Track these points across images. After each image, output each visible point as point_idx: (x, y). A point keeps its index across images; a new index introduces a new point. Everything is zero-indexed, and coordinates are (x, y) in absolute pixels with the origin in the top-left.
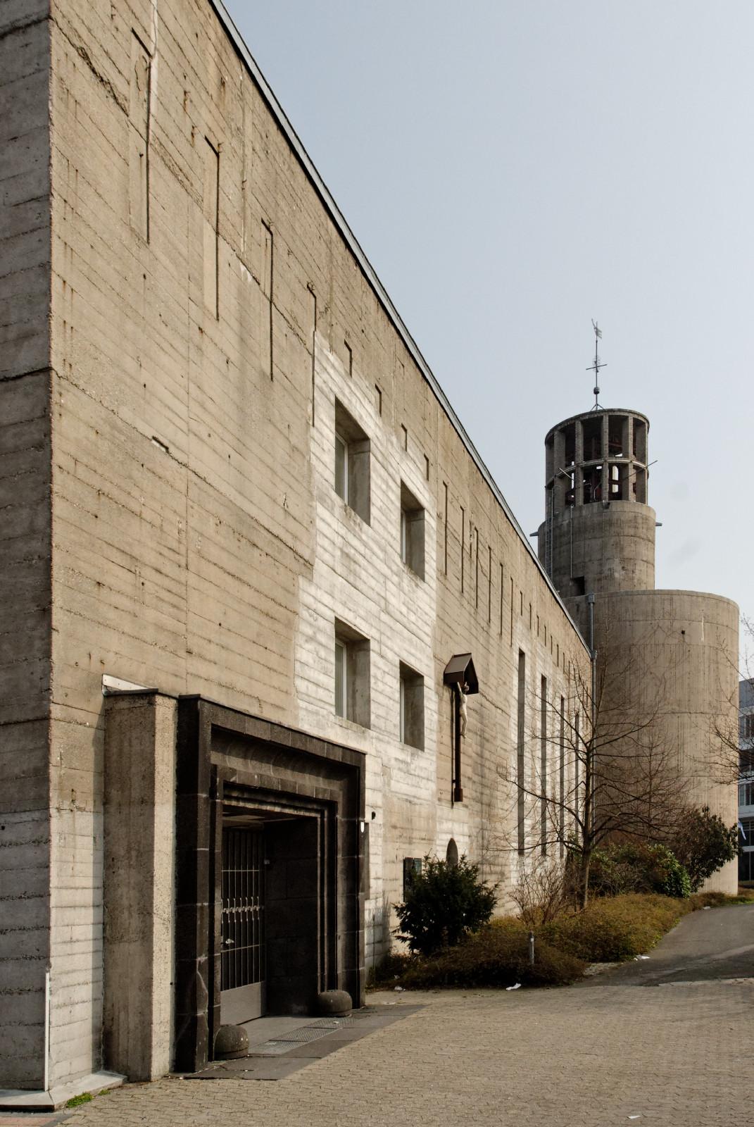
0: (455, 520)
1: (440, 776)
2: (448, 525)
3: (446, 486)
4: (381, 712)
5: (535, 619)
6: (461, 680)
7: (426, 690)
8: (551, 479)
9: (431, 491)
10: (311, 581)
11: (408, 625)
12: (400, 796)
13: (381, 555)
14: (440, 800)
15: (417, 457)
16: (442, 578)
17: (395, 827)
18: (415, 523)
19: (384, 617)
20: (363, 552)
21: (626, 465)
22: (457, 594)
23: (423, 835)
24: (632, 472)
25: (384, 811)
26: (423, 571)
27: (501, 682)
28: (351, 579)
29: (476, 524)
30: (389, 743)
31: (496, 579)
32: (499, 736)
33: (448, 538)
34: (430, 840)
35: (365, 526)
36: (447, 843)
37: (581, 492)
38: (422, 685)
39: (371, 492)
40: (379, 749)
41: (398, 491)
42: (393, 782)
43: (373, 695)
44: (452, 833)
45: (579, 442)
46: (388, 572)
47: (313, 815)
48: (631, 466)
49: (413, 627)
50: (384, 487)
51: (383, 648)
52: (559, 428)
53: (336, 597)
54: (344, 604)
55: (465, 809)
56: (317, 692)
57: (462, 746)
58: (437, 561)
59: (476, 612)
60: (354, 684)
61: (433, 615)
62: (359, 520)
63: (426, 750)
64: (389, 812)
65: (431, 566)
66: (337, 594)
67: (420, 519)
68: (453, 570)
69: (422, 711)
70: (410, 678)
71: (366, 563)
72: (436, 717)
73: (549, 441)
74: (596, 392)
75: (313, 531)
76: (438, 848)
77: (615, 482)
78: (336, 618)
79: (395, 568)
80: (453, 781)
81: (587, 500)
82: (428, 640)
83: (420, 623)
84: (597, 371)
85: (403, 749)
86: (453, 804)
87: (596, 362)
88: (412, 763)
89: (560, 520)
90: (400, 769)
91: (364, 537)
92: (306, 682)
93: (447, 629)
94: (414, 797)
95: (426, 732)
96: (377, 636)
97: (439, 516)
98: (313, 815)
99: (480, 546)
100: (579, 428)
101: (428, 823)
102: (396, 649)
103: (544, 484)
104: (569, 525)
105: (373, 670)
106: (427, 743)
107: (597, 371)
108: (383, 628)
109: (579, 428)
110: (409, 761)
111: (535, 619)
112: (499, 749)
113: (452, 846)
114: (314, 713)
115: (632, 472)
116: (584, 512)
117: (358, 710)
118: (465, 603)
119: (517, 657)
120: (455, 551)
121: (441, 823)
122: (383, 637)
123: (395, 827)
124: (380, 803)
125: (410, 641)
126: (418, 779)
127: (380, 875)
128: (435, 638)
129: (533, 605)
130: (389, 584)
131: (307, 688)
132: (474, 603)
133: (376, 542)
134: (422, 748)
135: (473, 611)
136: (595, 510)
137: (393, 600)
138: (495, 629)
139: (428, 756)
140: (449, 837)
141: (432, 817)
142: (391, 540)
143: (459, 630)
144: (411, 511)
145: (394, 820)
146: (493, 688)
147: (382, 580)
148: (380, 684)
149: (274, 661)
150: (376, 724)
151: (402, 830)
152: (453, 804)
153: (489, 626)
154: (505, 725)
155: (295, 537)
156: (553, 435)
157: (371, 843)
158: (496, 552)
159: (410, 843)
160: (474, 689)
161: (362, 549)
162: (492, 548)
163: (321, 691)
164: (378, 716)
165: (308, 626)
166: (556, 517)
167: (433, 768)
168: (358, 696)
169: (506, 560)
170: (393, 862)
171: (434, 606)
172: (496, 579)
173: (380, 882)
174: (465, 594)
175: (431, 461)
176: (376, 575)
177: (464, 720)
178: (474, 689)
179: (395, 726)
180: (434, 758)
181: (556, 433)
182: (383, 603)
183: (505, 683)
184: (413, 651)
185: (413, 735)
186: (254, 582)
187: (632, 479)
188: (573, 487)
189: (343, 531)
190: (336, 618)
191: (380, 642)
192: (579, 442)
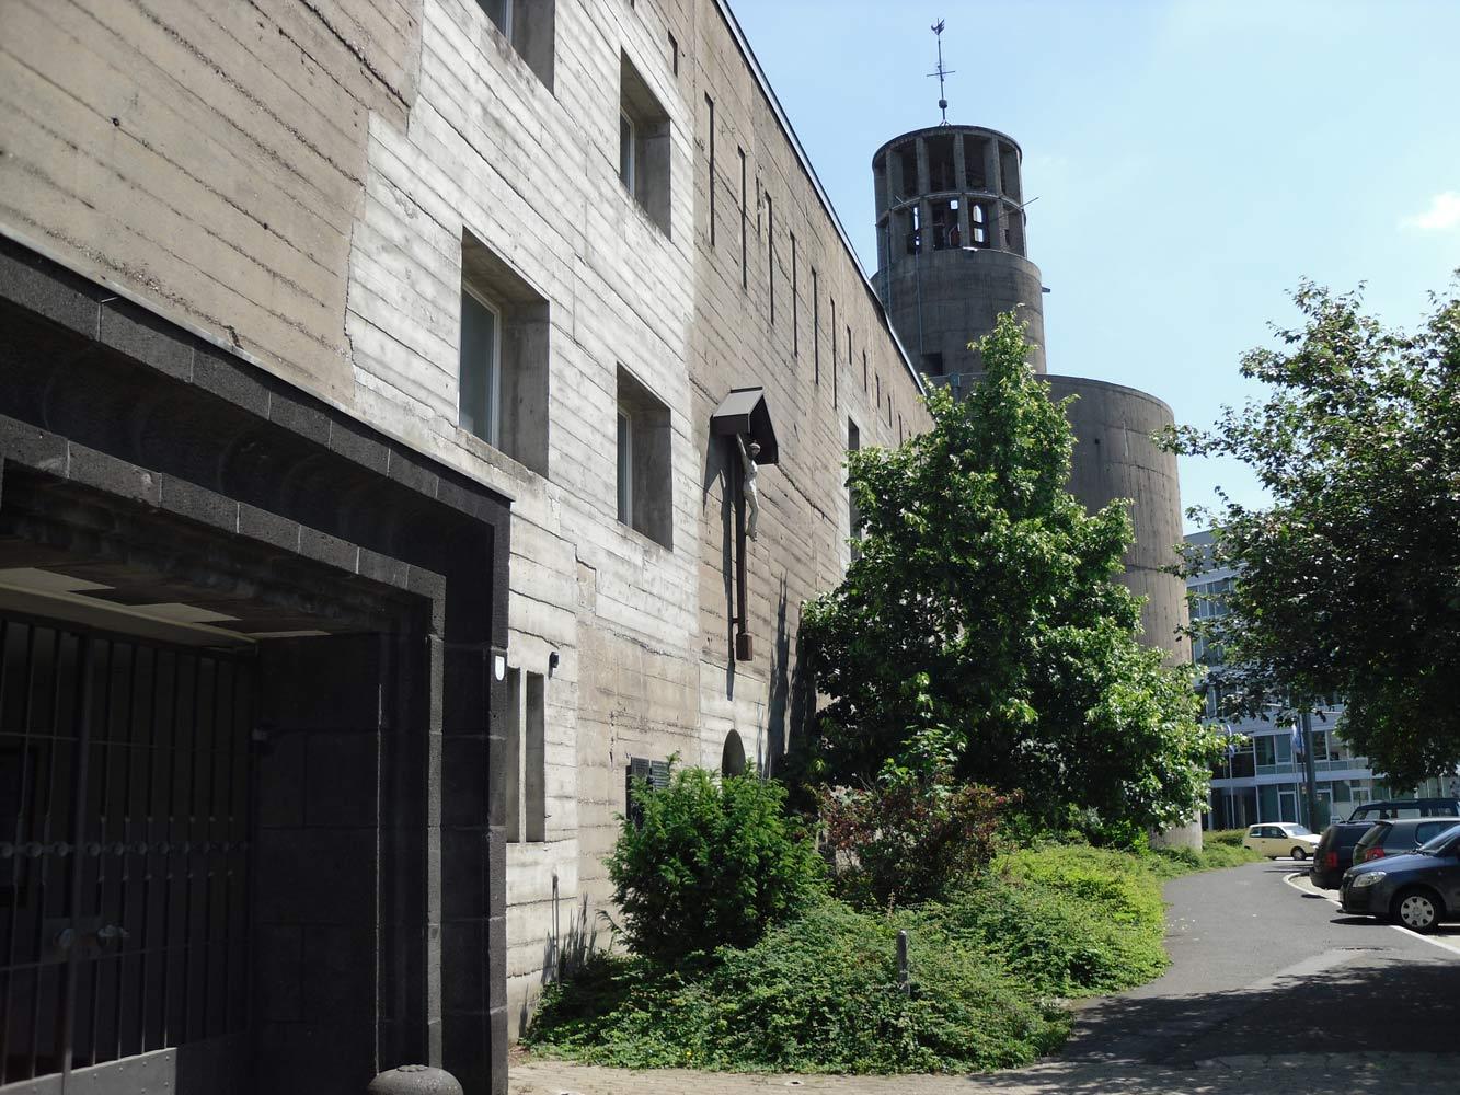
0: (729, 165)
1: (707, 606)
2: (715, 166)
3: (711, 104)
4: (576, 451)
5: (872, 380)
6: (741, 442)
7: (674, 436)
8: (884, 215)
9: (681, 94)
10: (403, 132)
11: (635, 304)
12: (618, 630)
13: (579, 157)
14: (706, 652)
15: (655, 28)
16: (705, 248)
17: (607, 692)
18: (651, 141)
19: (579, 267)
20: (538, 137)
21: (993, 202)
22: (736, 289)
23: (672, 716)
24: (1001, 212)
25: (581, 656)
26: (669, 221)
27: (819, 464)
28: (507, 171)
29: (767, 186)
30: (591, 517)
31: (805, 289)
32: (820, 557)
33: (716, 185)
34: (687, 731)
35: (541, 88)
36: (723, 739)
37: (928, 234)
38: (668, 425)
39: (557, 39)
40: (568, 523)
41: (617, 66)
42: (601, 600)
43: (553, 410)
44: (734, 720)
45: (922, 166)
46: (594, 195)
47: (401, 575)
48: (1000, 206)
49: (644, 311)
50: (586, 42)
51: (579, 306)
52: (892, 146)
53: (466, 188)
54: (488, 212)
55: (756, 677)
56: (408, 364)
57: (749, 559)
58: (697, 214)
59: (772, 330)
60: (515, 385)
61: (690, 307)
62: (527, 71)
63: (675, 549)
64: (592, 659)
65: (682, 218)
66: (469, 184)
67: (663, 136)
68: (729, 240)
69: (668, 475)
70: (641, 413)
71: (542, 156)
72: (694, 529)
73: (879, 163)
74: (943, 105)
75: (415, 42)
76: (704, 746)
77: (978, 225)
78: (466, 231)
79: (606, 189)
80: (732, 621)
81: (939, 244)
82: (679, 347)
83: (661, 310)
84: (942, 80)
85: (625, 537)
86: (732, 665)
87: (940, 67)
88: (644, 568)
89: (900, 270)
90: (621, 578)
91: (538, 106)
92: (379, 335)
93: (715, 338)
94: (650, 637)
95: (677, 517)
96: (566, 301)
97: (698, 144)
98: (401, 575)
99: (774, 223)
100: (920, 146)
101: (682, 695)
102: (610, 340)
103: (873, 221)
104: (914, 278)
105: (554, 363)
106: (677, 536)
107: (942, 80)
108: (579, 288)
109: (920, 146)
110: (640, 564)
111: (872, 380)
112: (819, 579)
113: (733, 744)
114: (399, 377)
115: (1001, 212)
116: (936, 262)
117: (522, 439)
118: (751, 308)
119: (846, 431)
120: (728, 213)
121: (710, 698)
122: (579, 306)
123: (607, 692)
124: (570, 637)
125: (642, 336)
126: (659, 604)
127: (569, 790)
128: (691, 346)
129: (868, 355)
130: (593, 212)
131: (382, 348)
132: (767, 313)
133: (568, 131)
134: (668, 546)
135: (765, 327)
136: (953, 261)
137: (600, 245)
138: (806, 371)
139: (680, 562)
140: (728, 727)
141: (690, 685)
142: (601, 141)
143: (739, 348)
144: (643, 122)
145: (605, 677)
146: (806, 470)
147: (579, 202)
148: (572, 395)
149: (286, 260)
150: (562, 472)
151: (620, 702)
152: (732, 665)
153: (796, 362)
154: (830, 541)
155: (366, 33)
156: (884, 155)
157: (547, 719)
158: (803, 244)
159: (644, 730)
160: (769, 454)
161: (535, 128)
162: (796, 236)
163: (418, 364)
164: (566, 456)
165: (392, 222)
166: (894, 267)
167: (691, 587)
168: (523, 410)
169: (821, 266)
170: (603, 765)
171: (692, 292)
172: (805, 289)
173: (571, 805)
174: (750, 292)
175: (682, 46)
176: (564, 186)
177: (753, 507)
178: (769, 454)
179: (606, 486)
180: (694, 570)
181: (888, 152)
182: (579, 243)
183: (826, 468)
184: (647, 355)
185: (646, 510)
186: (234, 70)
187: (1004, 223)
188: (916, 228)
189: (489, 75)
190: (466, 231)
191: (572, 314)
192: (922, 166)
